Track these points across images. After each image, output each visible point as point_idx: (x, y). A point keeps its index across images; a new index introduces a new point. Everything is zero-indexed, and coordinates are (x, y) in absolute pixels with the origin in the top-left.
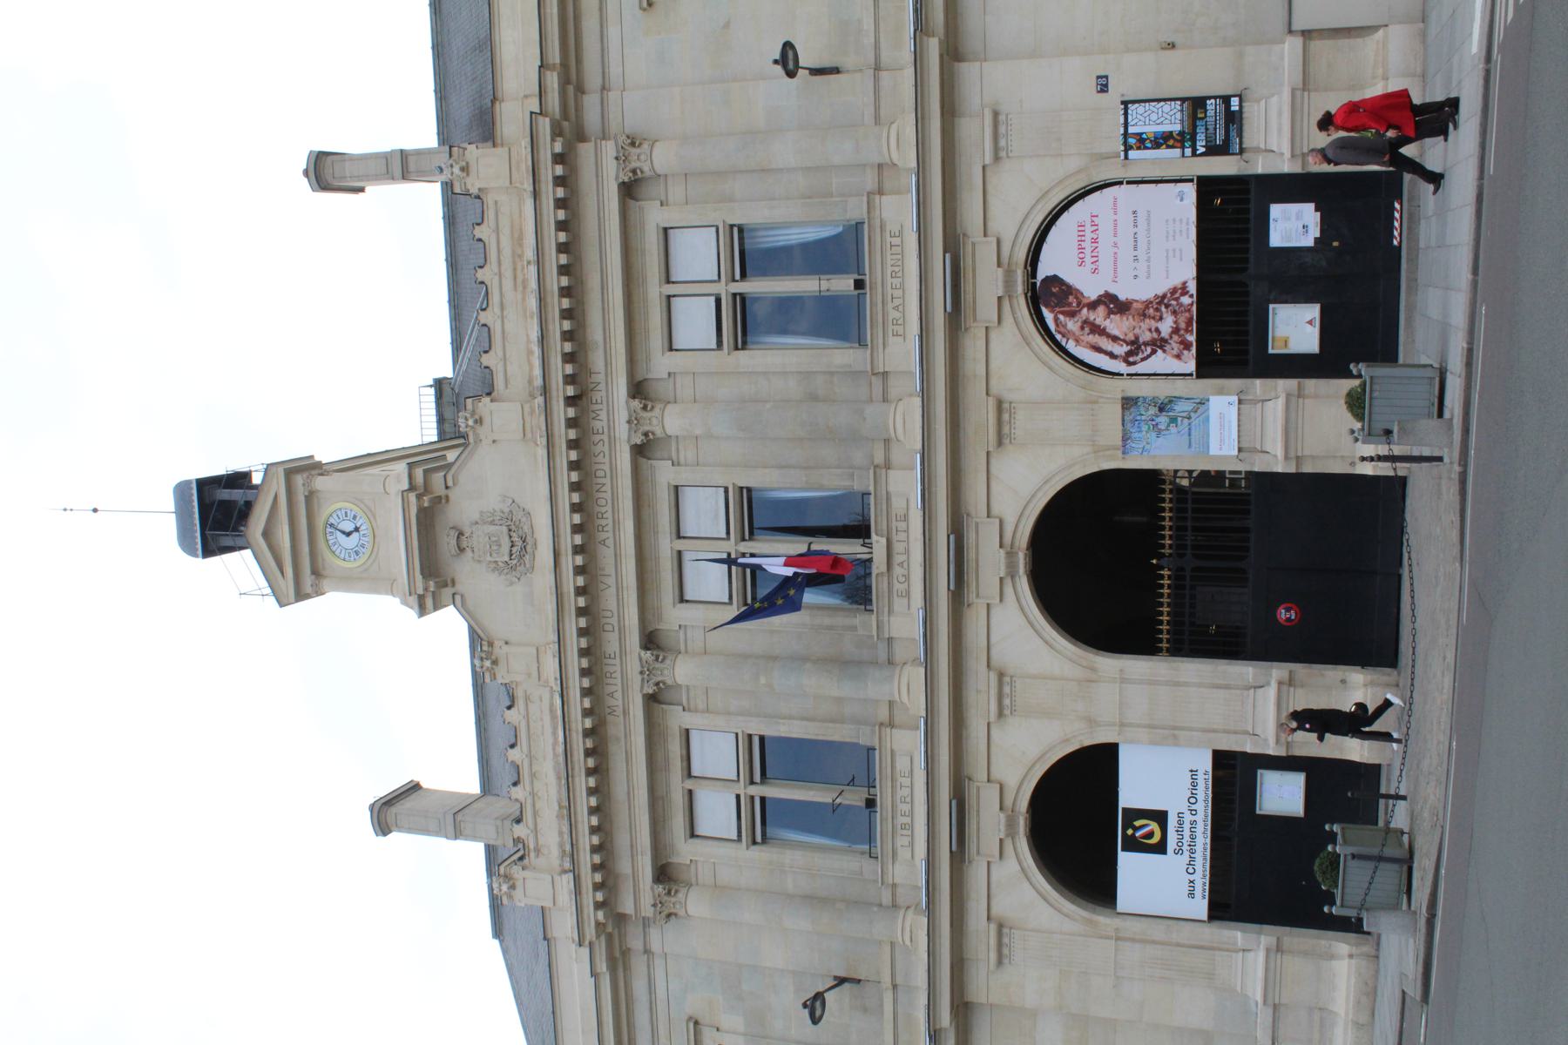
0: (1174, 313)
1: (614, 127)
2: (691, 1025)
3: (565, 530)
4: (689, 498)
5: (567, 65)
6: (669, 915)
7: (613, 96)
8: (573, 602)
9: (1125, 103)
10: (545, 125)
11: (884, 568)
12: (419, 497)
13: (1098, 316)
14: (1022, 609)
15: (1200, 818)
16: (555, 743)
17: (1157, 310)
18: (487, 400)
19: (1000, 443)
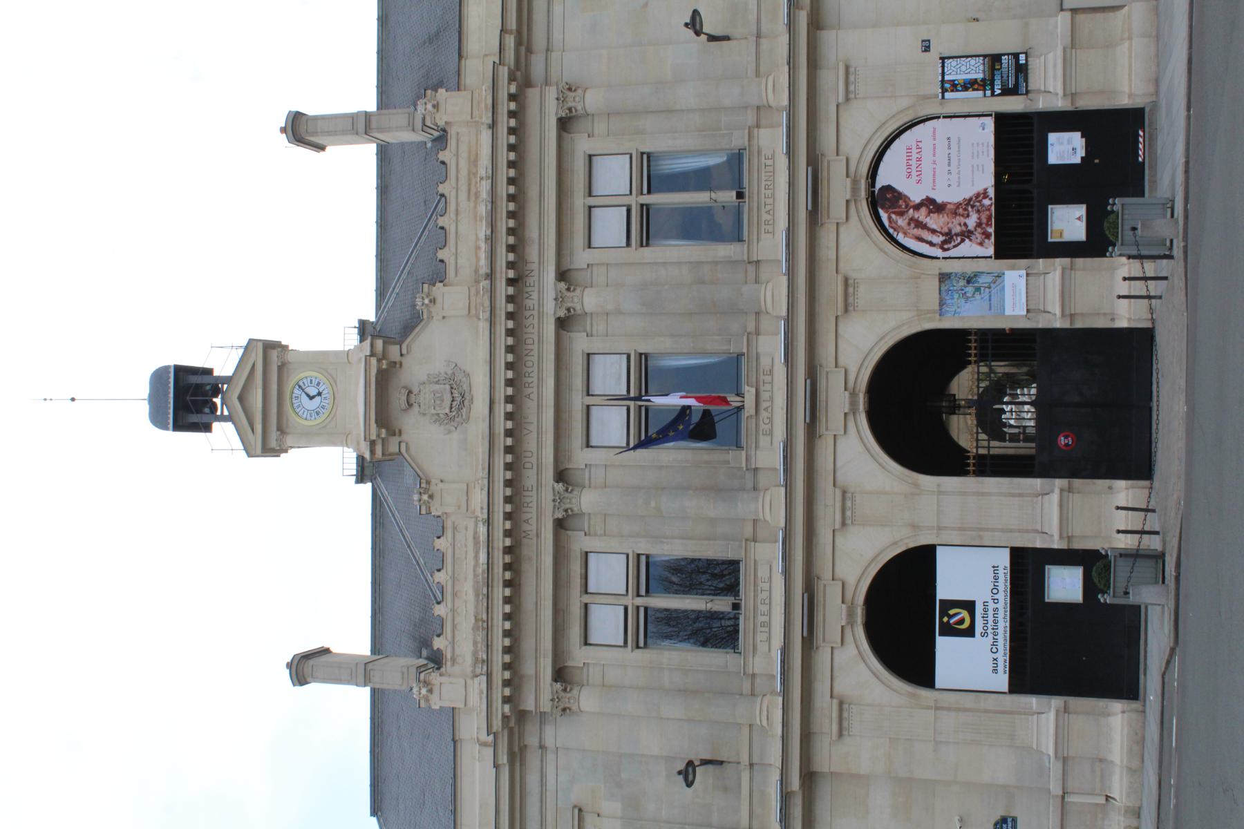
0: (978, 211)
1: (554, 76)
2: (576, 811)
3: (500, 383)
4: (599, 364)
5: (521, 33)
6: (564, 710)
7: (555, 56)
8: (502, 441)
9: (943, 59)
10: (504, 72)
11: (753, 412)
12: (379, 361)
13: (921, 215)
14: (861, 438)
15: (1001, 605)
16: (476, 565)
17: (965, 209)
18: (439, 285)
19: (846, 310)
